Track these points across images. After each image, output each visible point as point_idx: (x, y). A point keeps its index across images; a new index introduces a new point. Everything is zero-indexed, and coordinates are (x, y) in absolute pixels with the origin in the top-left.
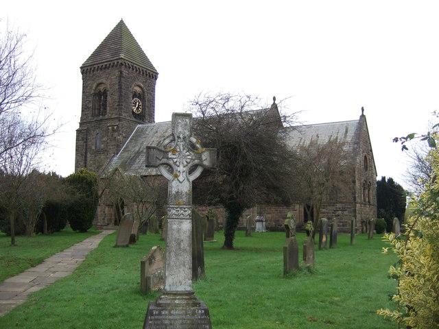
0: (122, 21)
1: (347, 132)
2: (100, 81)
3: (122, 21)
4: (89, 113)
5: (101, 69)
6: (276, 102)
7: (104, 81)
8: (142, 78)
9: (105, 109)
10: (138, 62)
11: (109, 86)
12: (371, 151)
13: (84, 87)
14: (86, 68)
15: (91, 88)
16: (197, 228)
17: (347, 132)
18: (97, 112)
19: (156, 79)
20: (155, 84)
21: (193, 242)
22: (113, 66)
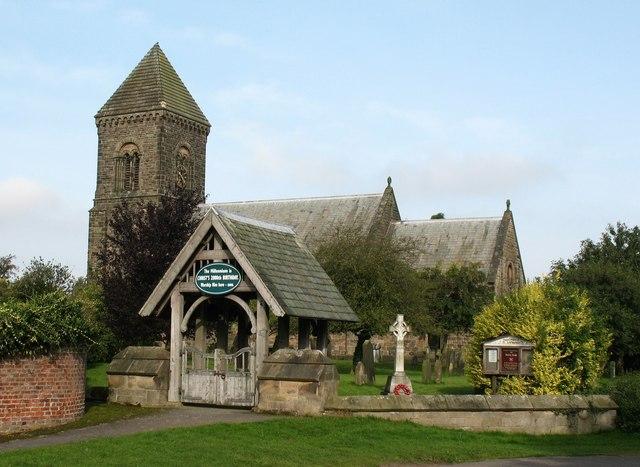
0: (157, 47)
1: (486, 233)
2: (128, 139)
3: (157, 47)
4: (109, 185)
5: (129, 122)
6: (392, 185)
7: (134, 139)
8: (189, 135)
9: (136, 181)
10: (183, 110)
11: (142, 149)
12: (519, 257)
13: (102, 147)
14: (104, 119)
15: (113, 149)
16: (407, 435)
17: (486, 233)
18: (122, 185)
19: (207, 134)
20: (205, 142)
21: (413, 424)
22: (148, 120)
